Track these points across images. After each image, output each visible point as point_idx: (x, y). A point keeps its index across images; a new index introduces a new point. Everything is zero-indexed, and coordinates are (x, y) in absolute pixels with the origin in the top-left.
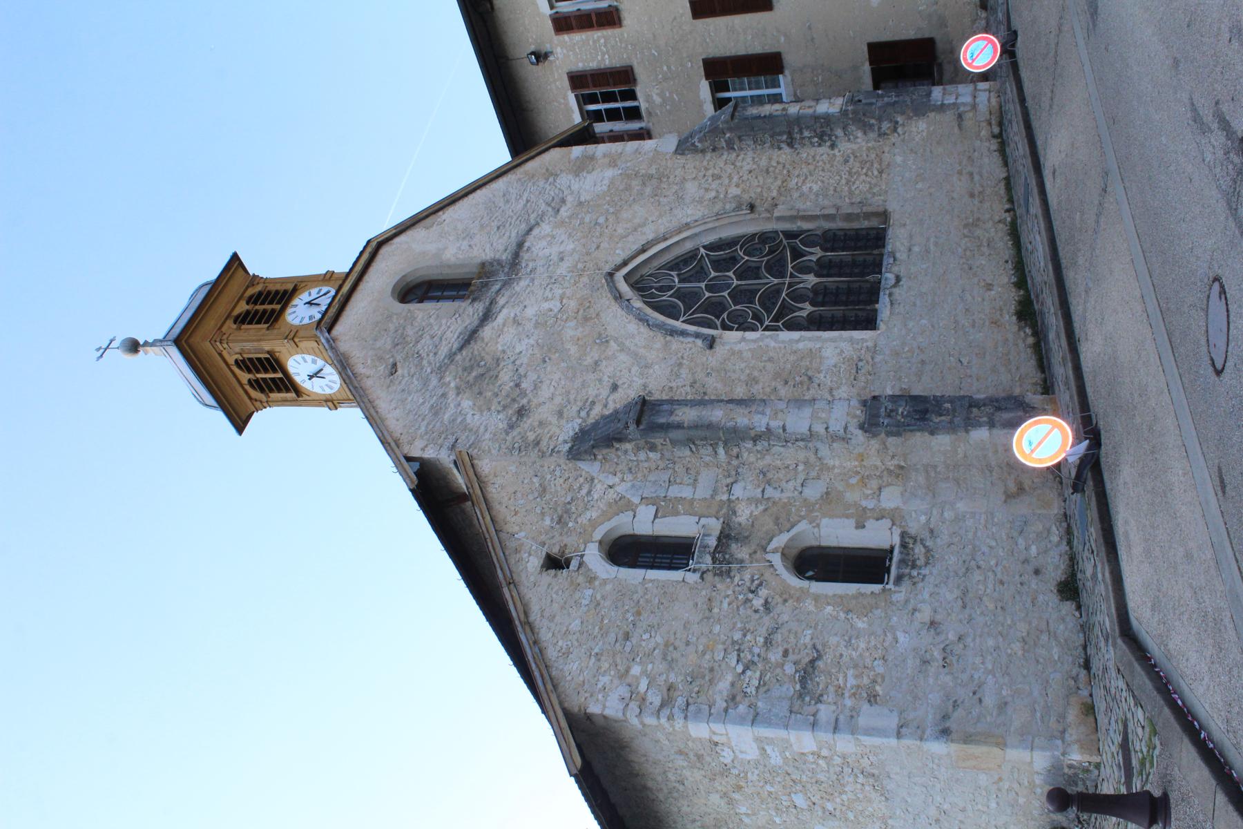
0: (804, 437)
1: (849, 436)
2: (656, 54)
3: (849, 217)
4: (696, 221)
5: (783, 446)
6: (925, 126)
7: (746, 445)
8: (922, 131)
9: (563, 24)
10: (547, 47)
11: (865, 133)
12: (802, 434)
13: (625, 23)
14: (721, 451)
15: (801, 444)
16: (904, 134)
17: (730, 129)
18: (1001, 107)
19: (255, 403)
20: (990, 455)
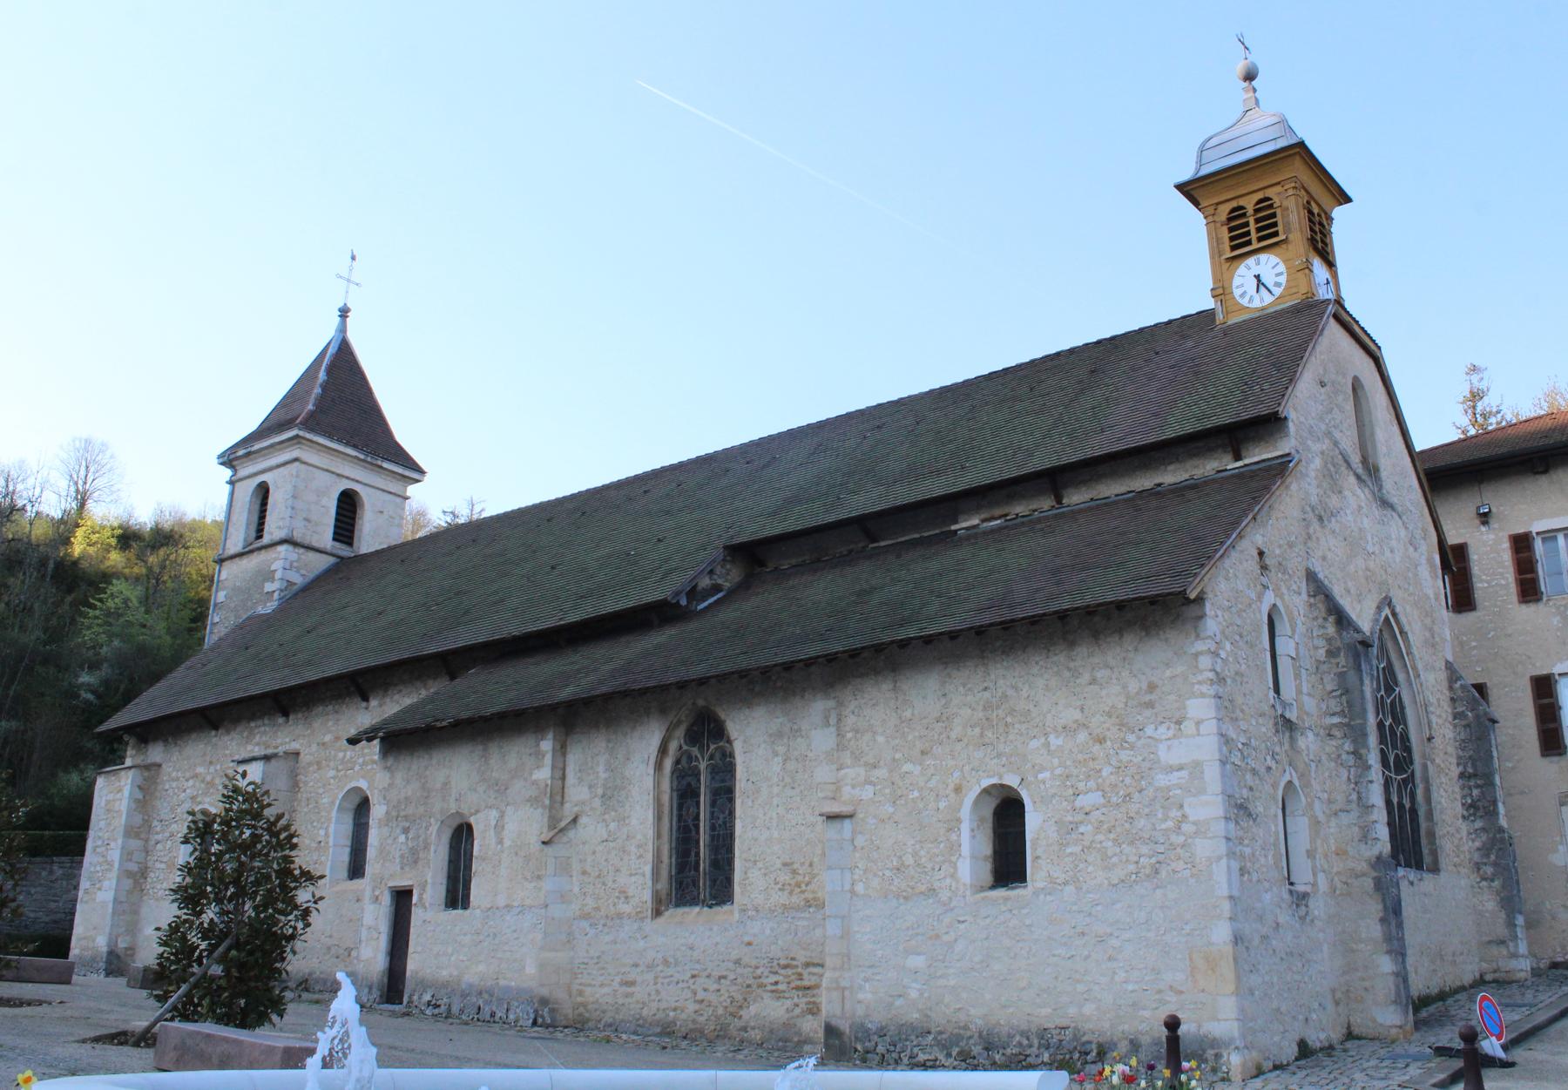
0: (1364, 800)
1: (1370, 842)
2: (1490, 636)
3: (1432, 835)
4: (1421, 685)
5: (1349, 779)
6: (1490, 908)
7: (1347, 745)
8: (1484, 905)
9: (1521, 544)
10: (1494, 524)
11: (1478, 849)
12: (1368, 799)
13: (1524, 606)
14: (1336, 720)
15: (1354, 797)
16: (1479, 887)
17: (1477, 717)
18: (1516, 982)
19: (1213, 207)
20: (1359, 974)
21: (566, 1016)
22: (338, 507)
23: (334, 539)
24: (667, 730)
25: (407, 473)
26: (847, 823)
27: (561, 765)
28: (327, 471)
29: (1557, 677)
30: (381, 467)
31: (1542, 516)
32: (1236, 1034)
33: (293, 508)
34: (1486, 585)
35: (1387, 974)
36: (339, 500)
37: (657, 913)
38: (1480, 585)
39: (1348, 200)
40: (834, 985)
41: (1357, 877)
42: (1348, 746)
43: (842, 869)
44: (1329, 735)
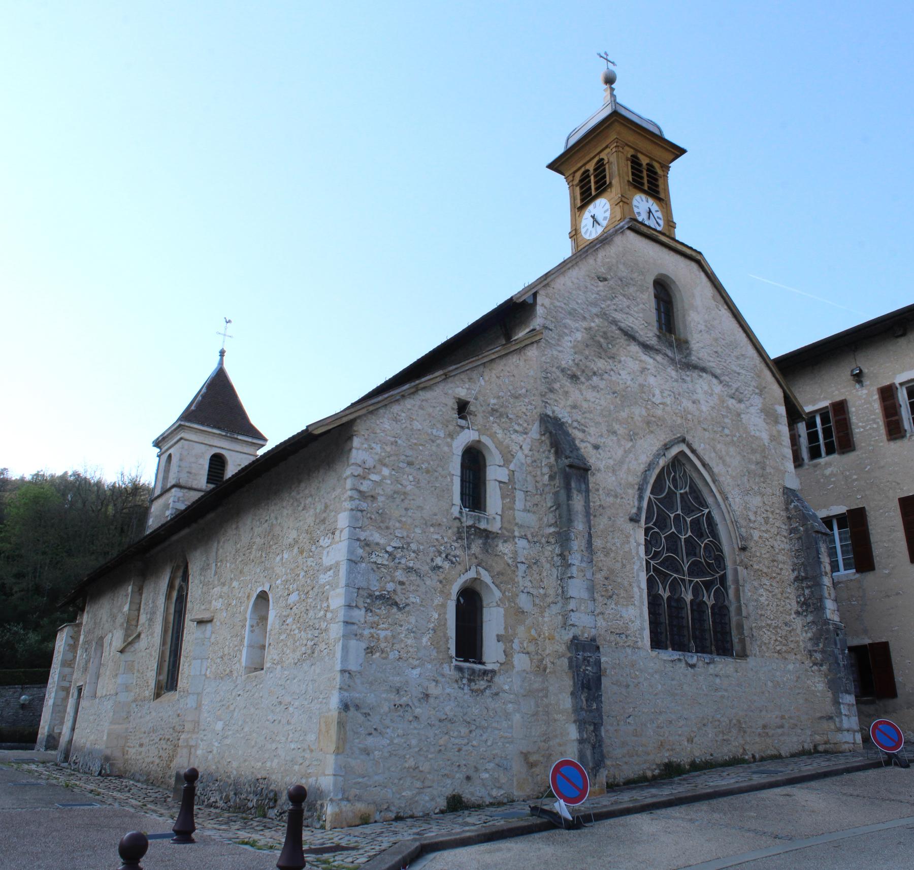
4: (730, 505)
8: (816, 687)
9: (887, 394)
10: (867, 382)
11: (810, 639)
14: (552, 530)
15: (560, 591)
16: (812, 671)
17: (806, 531)
18: (841, 752)
20: (558, 740)
22: (210, 463)
23: (208, 482)
25: (255, 441)
26: (209, 626)
30: (237, 439)
33: (179, 466)
34: (862, 430)
35: (574, 740)
38: (857, 431)
39: (682, 151)
41: (559, 657)
43: (202, 659)
44: (548, 542)
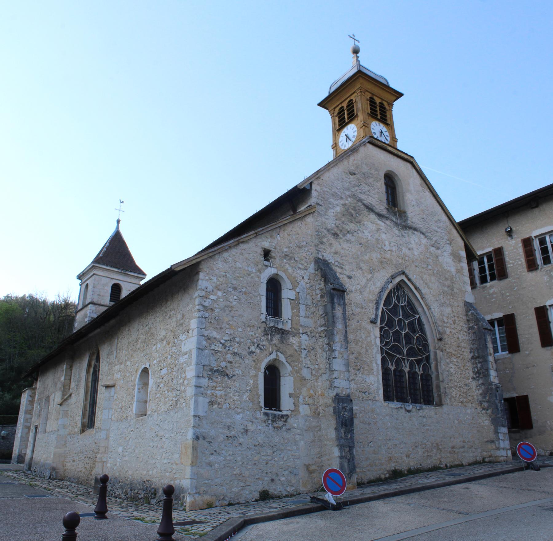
1: (332, 389)
2: (515, 289)
4: (432, 313)
5: (326, 357)
8: (484, 423)
9: (527, 243)
10: (515, 236)
11: (481, 394)
14: (322, 328)
15: (328, 366)
16: (482, 414)
17: (478, 328)
18: (499, 462)
20: (327, 457)
21: (61, 476)
22: (112, 289)
23: (110, 301)
24: (90, 357)
25: (139, 276)
26: (113, 389)
27: (69, 374)
28: (107, 277)
29: (548, 307)
30: (128, 274)
31: (537, 228)
32: (189, 487)
34: (512, 265)
36: (112, 287)
37: (83, 431)
40: (100, 460)
41: (328, 407)
42: (326, 342)
44: (320, 336)
